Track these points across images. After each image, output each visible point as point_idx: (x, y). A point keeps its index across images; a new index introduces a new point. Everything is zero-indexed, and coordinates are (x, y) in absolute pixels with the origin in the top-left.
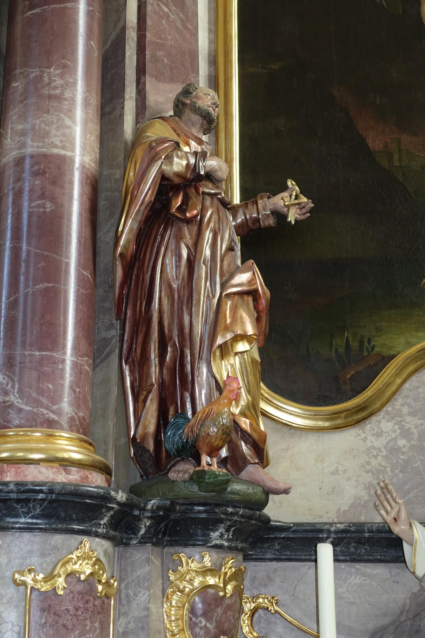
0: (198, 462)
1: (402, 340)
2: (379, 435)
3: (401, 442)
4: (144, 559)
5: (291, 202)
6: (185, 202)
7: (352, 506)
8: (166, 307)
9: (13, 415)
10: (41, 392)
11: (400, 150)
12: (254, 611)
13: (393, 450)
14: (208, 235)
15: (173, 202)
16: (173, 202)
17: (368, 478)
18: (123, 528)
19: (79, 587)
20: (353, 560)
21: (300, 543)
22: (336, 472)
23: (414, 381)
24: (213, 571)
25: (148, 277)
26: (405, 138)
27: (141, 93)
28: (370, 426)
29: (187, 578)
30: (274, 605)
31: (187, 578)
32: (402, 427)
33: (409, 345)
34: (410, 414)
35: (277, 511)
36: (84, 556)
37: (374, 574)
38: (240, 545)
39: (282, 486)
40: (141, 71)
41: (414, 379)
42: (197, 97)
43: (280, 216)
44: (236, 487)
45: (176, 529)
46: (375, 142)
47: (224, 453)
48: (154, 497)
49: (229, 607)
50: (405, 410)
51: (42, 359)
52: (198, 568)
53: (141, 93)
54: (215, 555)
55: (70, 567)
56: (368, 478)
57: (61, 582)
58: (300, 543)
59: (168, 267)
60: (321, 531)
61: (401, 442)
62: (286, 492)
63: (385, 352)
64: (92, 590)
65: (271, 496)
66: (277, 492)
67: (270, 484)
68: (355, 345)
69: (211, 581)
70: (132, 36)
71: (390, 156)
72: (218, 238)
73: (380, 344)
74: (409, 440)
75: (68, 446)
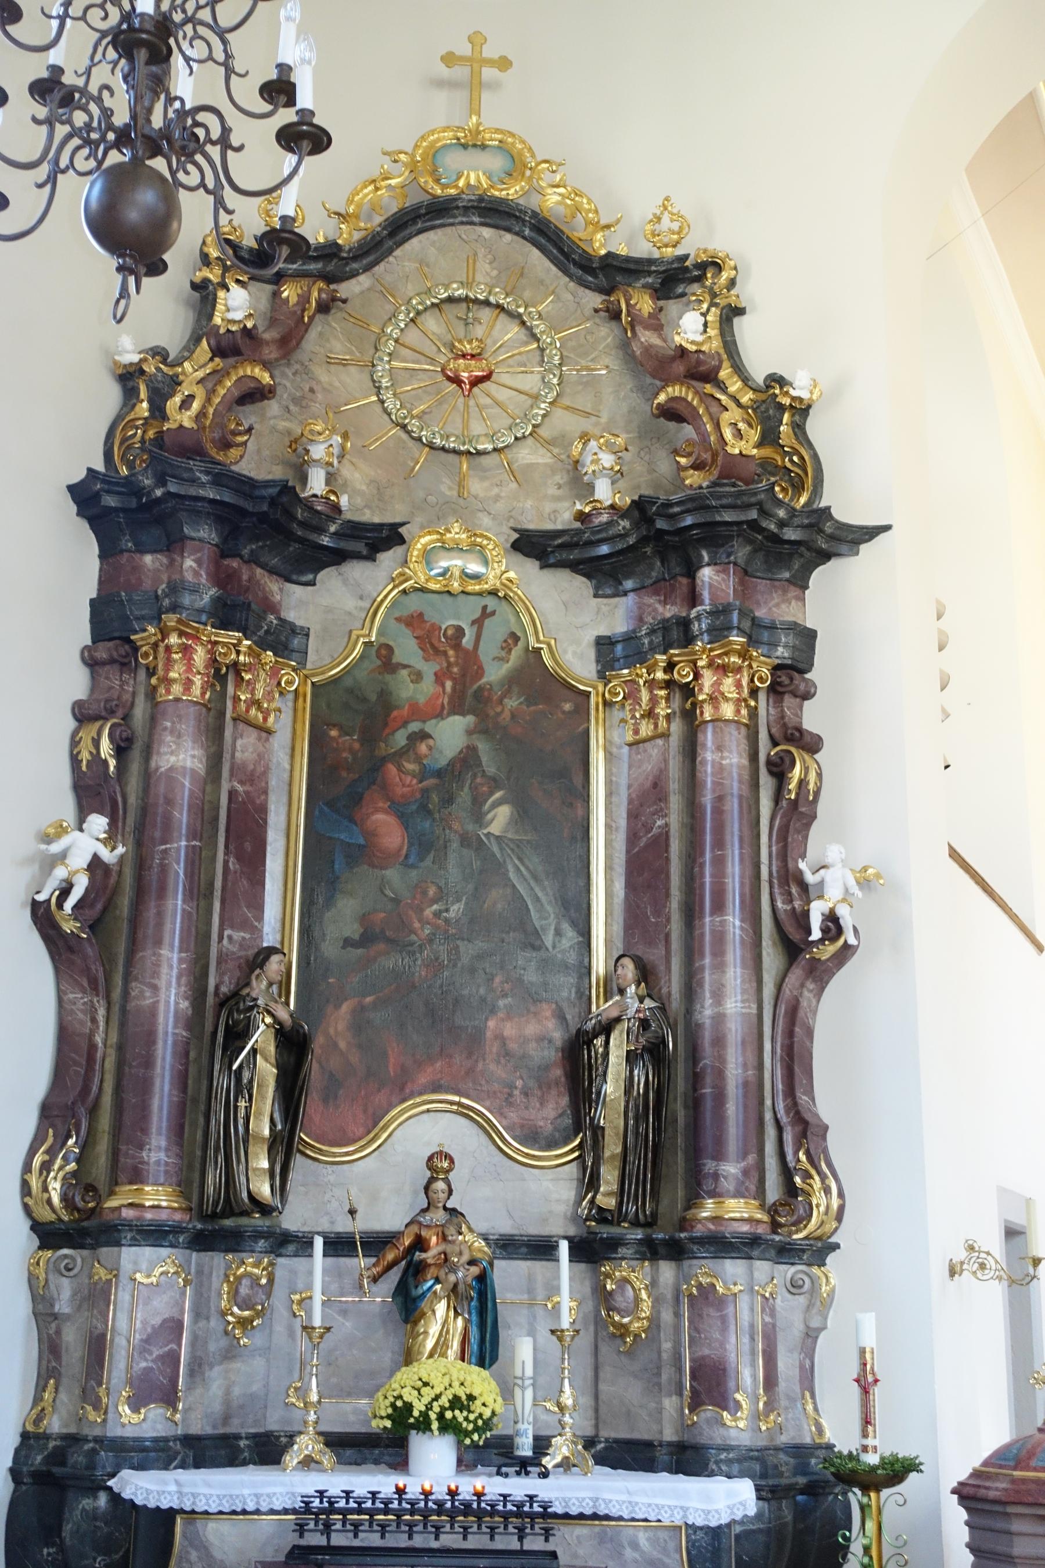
24: (256, 1265)
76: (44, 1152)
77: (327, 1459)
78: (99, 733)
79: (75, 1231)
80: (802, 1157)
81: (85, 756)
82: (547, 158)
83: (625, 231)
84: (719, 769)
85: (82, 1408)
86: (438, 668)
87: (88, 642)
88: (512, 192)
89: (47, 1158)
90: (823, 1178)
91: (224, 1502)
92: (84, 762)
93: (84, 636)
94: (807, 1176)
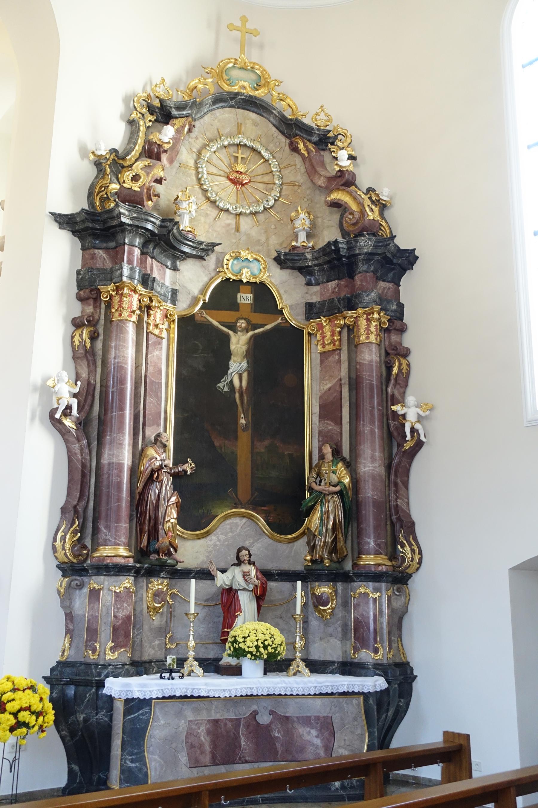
0: (159, 555)
1: (220, 511)
2: (211, 540)
3: (218, 543)
4: (143, 581)
5: (189, 467)
6: (158, 475)
7: (202, 562)
8: (151, 508)
9: (108, 542)
10: (116, 535)
11: (225, 446)
12: (171, 594)
13: (215, 545)
14: (164, 486)
15: (153, 477)
16: (153, 477)
17: (207, 554)
18: (138, 573)
19: (126, 590)
20: (201, 579)
21: (186, 574)
22: (197, 552)
23: (223, 524)
24: (162, 584)
25: (146, 499)
26: (226, 442)
27: (144, 432)
28: (208, 538)
29: (336, 664)
30: (98, 651)
31: (336, 664)
32: (218, 539)
33: (222, 512)
34: (221, 534)
35: (179, 566)
36: (127, 582)
37: (206, 583)
38: (169, 576)
39: (182, 560)
40: (144, 424)
41: (223, 523)
42: (162, 438)
43: (185, 471)
44: (169, 561)
45: (151, 573)
46: (217, 444)
47: (167, 552)
48: (146, 564)
49: (165, 594)
50: (220, 533)
51: (117, 526)
52: (158, 584)
53: (144, 432)
54: (162, 579)
55: (124, 586)
56: (207, 554)
57: (122, 589)
58: (186, 574)
59: (152, 495)
60: (192, 570)
61: (218, 543)
62: (183, 562)
63: (215, 514)
64: (129, 591)
65: (179, 563)
66: (180, 562)
67: (178, 560)
68: (206, 512)
69: (160, 587)
70: (142, 412)
71: (221, 448)
72: (167, 480)
73: (214, 512)
74: (220, 542)
75: (123, 551)
76: (62, 532)
77: (199, 671)
78: (82, 332)
79: (77, 568)
80: (171, 93)
81: (77, 343)
82: (276, 79)
83: (309, 113)
84: (372, 422)
85: (87, 652)
86: (120, 153)
87: (77, 291)
88: (260, 93)
89: (63, 534)
90: (410, 545)
91: (153, 693)
92: (77, 346)
93: (75, 290)
94: (356, 192)
